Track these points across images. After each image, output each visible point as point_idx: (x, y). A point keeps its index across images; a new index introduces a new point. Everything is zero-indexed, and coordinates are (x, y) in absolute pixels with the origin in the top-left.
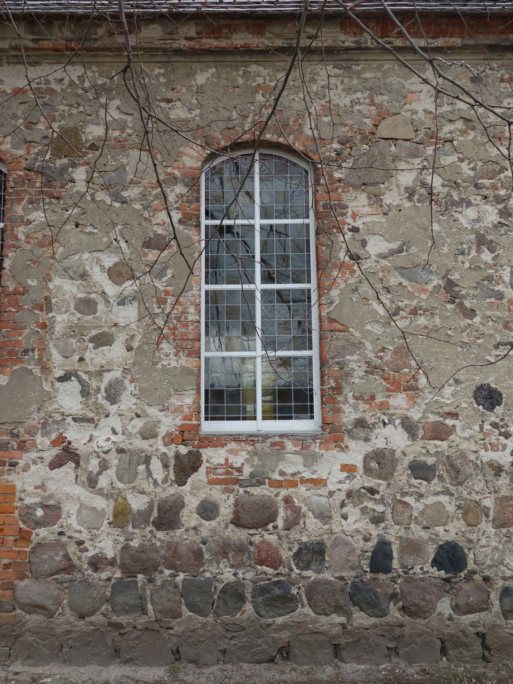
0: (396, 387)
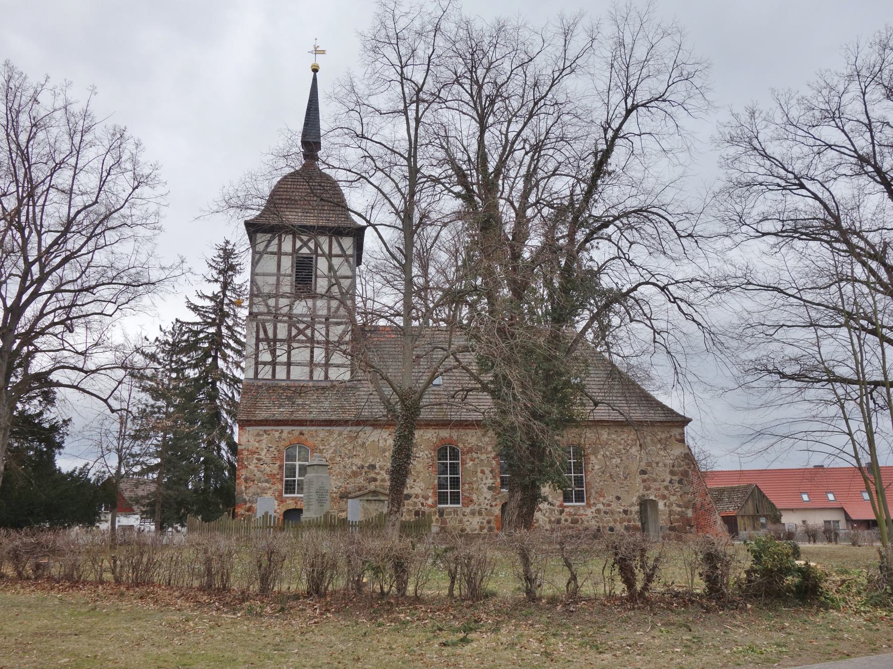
0: (601, 496)
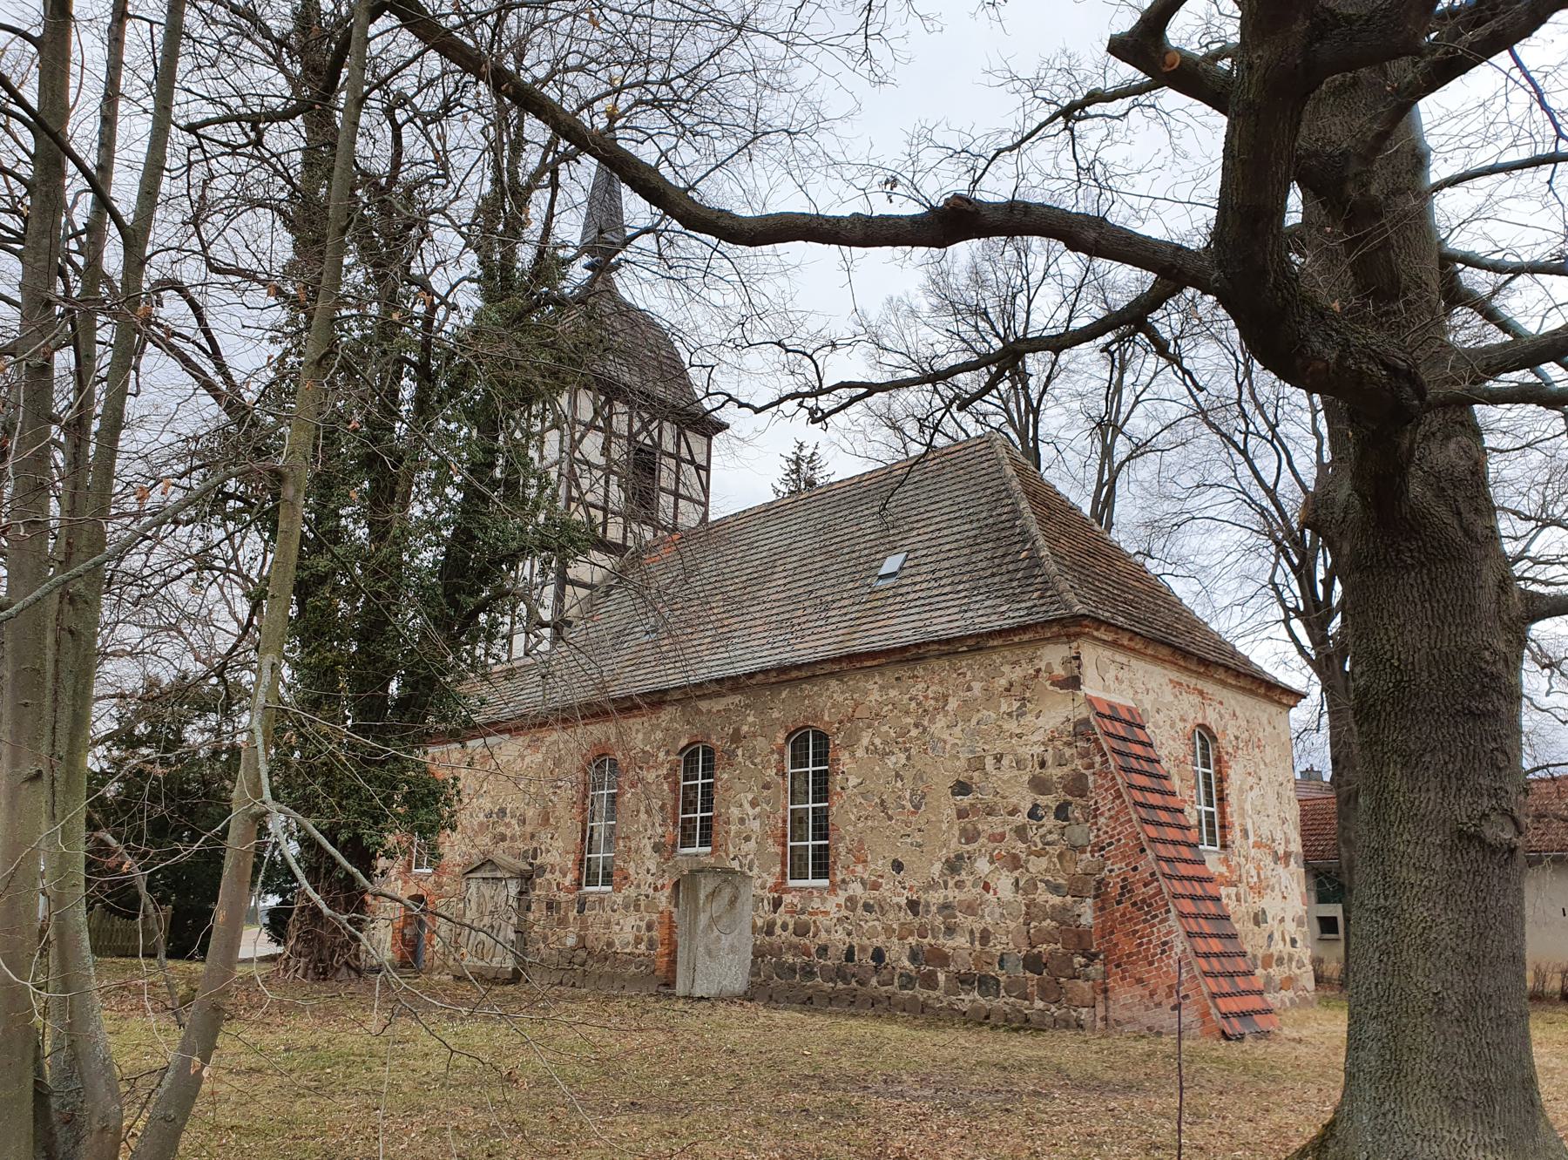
0: (858, 861)
